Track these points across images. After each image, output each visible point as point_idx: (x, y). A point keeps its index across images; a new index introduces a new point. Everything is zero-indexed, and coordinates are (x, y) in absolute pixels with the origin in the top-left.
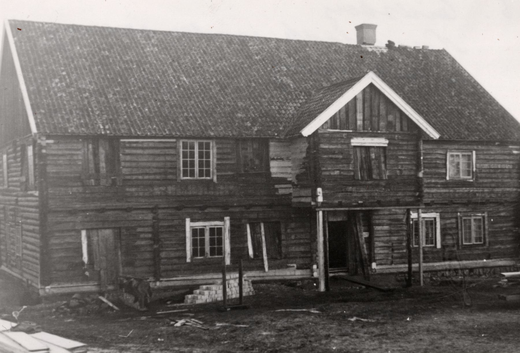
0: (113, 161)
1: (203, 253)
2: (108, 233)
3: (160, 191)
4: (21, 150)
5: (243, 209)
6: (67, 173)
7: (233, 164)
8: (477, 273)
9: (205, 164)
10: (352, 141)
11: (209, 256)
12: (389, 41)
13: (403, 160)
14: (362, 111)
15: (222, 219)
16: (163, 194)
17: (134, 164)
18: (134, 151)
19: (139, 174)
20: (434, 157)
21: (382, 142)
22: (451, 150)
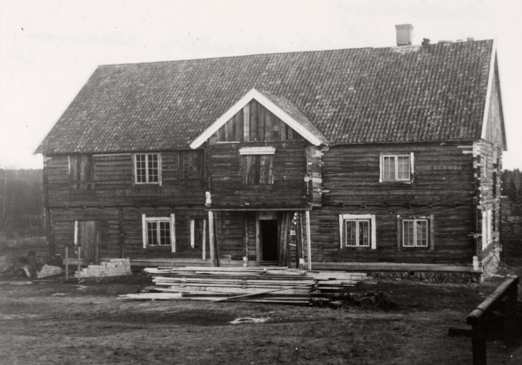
0: (89, 171)
1: (155, 242)
2: (92, 223)
3: (120, 193)
5: (187, 208)
6: (60, 180)
7: (176, 172)
8: (419, 276)
9: (153, 172)
10: (240, 150)
11: (160, 244)
12: (425, 39)
13: (290, 166)
15: (169, 216)
16: (122, 195)
17: (103, 173)
18: (103, 164)
19: (107, 181)
20: (365, 160)
21: (270, 150)
22: (384, 153)
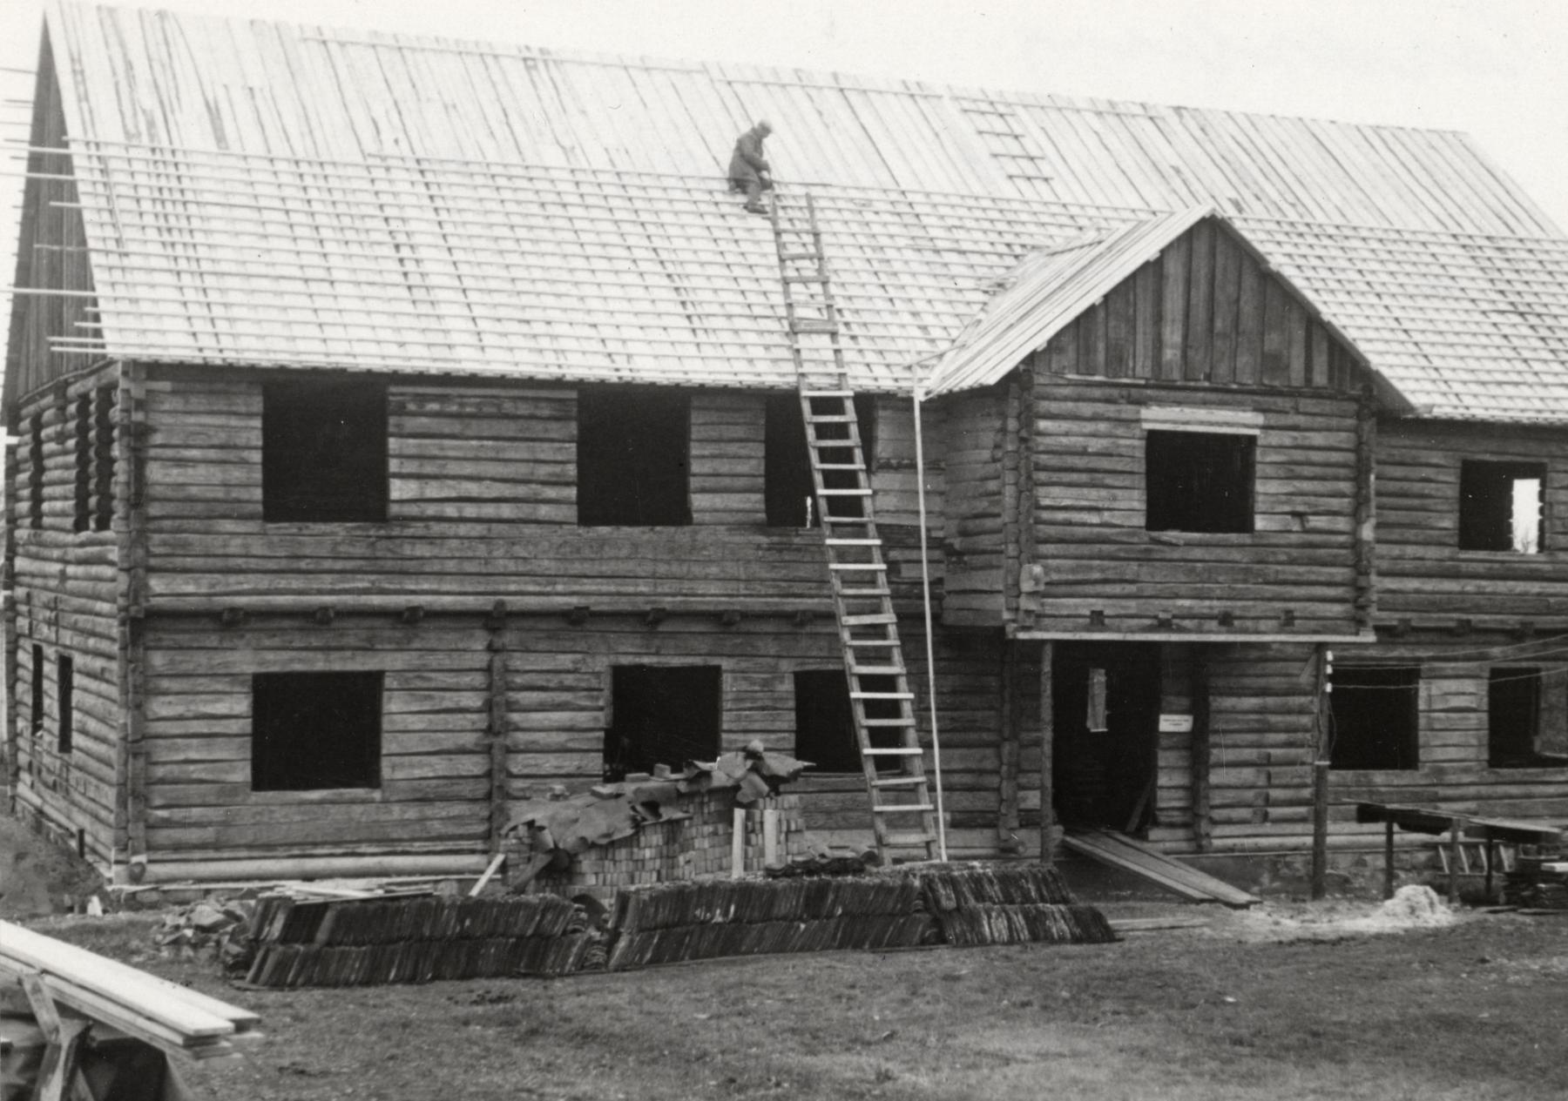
4: (79, 409)
14: (1179, 316)
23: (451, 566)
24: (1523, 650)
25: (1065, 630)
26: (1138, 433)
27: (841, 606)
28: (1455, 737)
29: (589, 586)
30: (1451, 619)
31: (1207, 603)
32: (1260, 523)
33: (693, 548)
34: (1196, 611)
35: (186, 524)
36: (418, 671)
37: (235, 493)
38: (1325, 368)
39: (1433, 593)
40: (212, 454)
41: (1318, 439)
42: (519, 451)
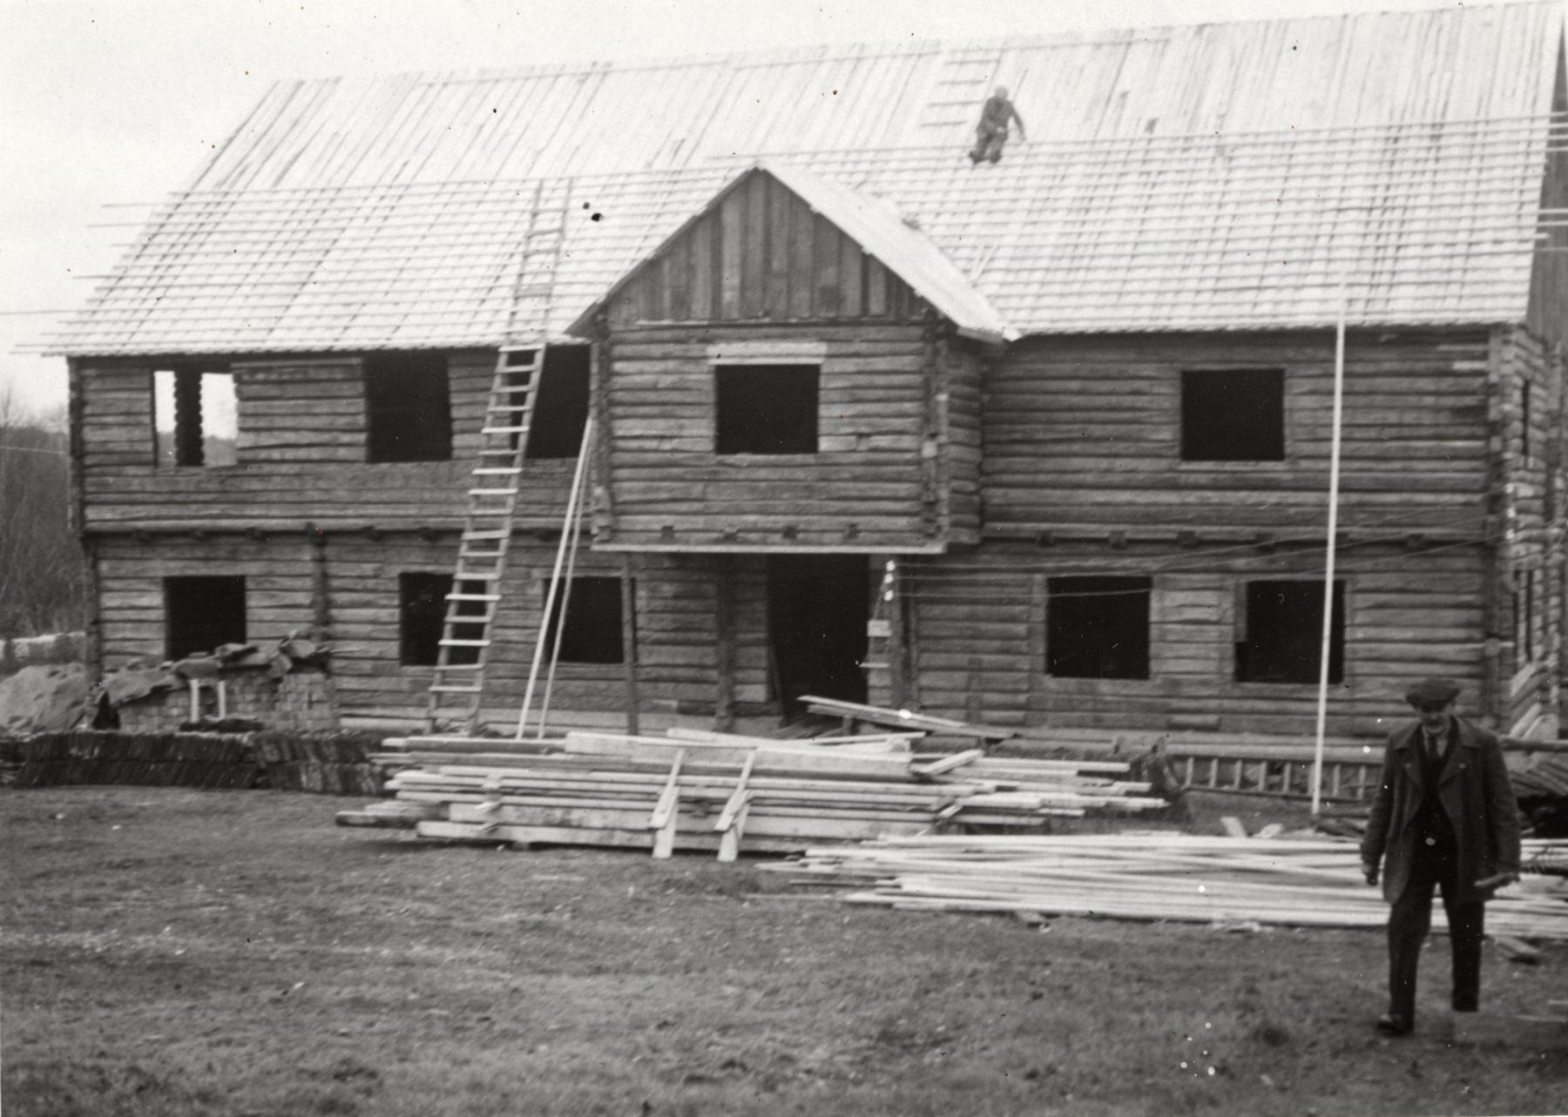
23: (275, 496)
24: (1273, 561)
25: (639, 543)
26: (706, 369)
27: (468, 523)
28: (1191, 650)
29: (371, 510)
30: (1170, 531)
31: (772, 518)
32: (824, 444)
33: (450, 480)
34: (760, 525)
35: (106, 470)
36: (268, 575)
37: (138, 447)
38: (882, 297)
39: (1148, 505)
40: (121, 419)
41: (881, 364)
42: (323, 407)
